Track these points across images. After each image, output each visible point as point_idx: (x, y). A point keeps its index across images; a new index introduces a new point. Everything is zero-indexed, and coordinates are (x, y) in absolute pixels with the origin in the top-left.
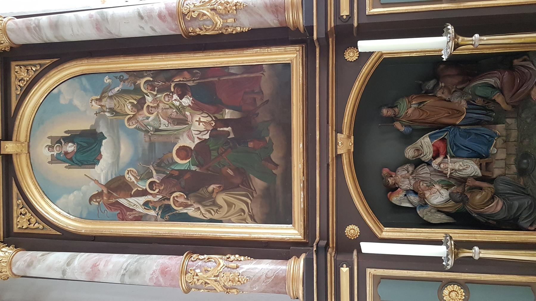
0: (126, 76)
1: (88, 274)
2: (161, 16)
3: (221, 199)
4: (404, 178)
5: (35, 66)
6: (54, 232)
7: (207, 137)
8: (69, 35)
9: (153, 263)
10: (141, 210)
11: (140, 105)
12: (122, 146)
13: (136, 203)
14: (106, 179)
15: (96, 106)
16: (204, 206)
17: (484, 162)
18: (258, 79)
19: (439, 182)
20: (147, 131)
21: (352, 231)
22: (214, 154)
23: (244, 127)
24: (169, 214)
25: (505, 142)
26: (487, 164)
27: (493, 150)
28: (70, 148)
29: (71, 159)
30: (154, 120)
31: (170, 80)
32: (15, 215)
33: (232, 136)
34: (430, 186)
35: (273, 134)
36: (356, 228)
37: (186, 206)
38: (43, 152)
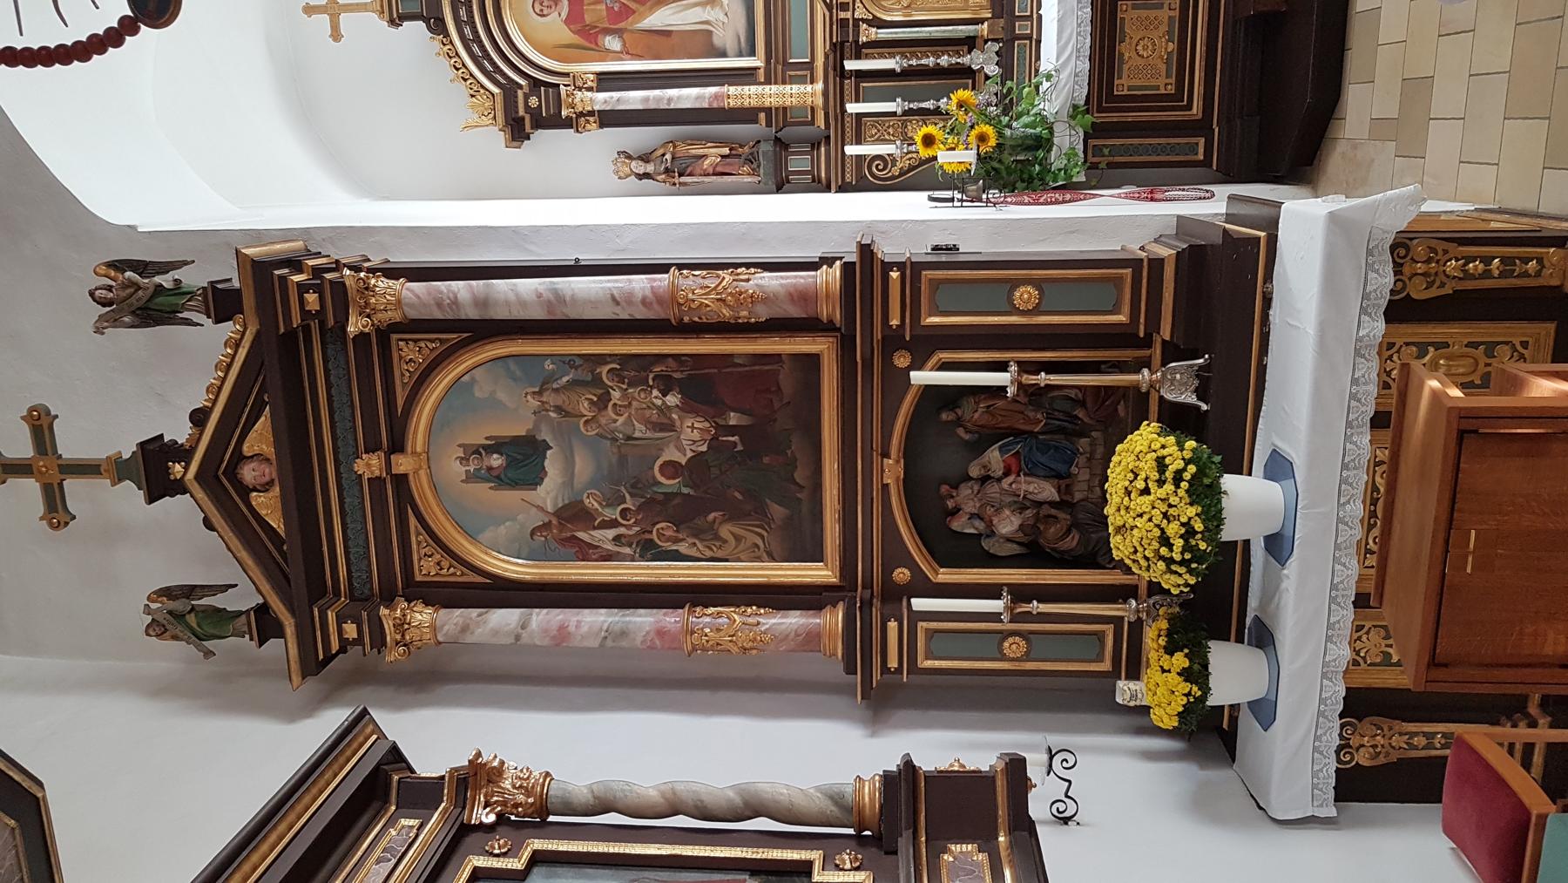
0: (578, 362)
1: (554, 638)
2: (644, 302)
3: (725, 531)
4: (966, 498)
5: (432, 341)
6: (480, 579)
7: (704, 448)
8: (501, 314)
9: (643, 620)
10: (610, 547)
11: (603, 401)
12: (577, 459)
13: (603, 537)
14: (555, 504)
15: (534, 403)
16: (702, 540)
17: (1063, 483)
18: (776, 373)
19: (1009, 505)
20: (615, 440)
21: (902, 575)
22: (715, 471)
23: (758, 439)
24: (650, 550)
25: (1089, 460)
26: (1067, 486)
27: (1074, 470)
28: (496, 461)
29: (498, 477)
30: (624, 424)
31: (647, 369)
32: (415, 558)
33: (740, 448)
34: (998, 511)
35: (797, 445)
36: (906, 571)
37: (676, 541)
38: (453, 468)
